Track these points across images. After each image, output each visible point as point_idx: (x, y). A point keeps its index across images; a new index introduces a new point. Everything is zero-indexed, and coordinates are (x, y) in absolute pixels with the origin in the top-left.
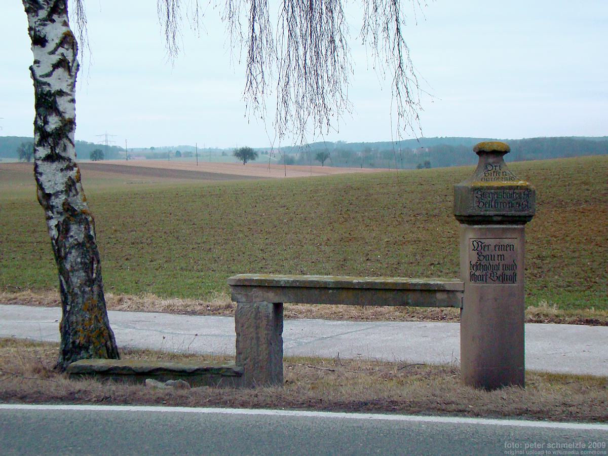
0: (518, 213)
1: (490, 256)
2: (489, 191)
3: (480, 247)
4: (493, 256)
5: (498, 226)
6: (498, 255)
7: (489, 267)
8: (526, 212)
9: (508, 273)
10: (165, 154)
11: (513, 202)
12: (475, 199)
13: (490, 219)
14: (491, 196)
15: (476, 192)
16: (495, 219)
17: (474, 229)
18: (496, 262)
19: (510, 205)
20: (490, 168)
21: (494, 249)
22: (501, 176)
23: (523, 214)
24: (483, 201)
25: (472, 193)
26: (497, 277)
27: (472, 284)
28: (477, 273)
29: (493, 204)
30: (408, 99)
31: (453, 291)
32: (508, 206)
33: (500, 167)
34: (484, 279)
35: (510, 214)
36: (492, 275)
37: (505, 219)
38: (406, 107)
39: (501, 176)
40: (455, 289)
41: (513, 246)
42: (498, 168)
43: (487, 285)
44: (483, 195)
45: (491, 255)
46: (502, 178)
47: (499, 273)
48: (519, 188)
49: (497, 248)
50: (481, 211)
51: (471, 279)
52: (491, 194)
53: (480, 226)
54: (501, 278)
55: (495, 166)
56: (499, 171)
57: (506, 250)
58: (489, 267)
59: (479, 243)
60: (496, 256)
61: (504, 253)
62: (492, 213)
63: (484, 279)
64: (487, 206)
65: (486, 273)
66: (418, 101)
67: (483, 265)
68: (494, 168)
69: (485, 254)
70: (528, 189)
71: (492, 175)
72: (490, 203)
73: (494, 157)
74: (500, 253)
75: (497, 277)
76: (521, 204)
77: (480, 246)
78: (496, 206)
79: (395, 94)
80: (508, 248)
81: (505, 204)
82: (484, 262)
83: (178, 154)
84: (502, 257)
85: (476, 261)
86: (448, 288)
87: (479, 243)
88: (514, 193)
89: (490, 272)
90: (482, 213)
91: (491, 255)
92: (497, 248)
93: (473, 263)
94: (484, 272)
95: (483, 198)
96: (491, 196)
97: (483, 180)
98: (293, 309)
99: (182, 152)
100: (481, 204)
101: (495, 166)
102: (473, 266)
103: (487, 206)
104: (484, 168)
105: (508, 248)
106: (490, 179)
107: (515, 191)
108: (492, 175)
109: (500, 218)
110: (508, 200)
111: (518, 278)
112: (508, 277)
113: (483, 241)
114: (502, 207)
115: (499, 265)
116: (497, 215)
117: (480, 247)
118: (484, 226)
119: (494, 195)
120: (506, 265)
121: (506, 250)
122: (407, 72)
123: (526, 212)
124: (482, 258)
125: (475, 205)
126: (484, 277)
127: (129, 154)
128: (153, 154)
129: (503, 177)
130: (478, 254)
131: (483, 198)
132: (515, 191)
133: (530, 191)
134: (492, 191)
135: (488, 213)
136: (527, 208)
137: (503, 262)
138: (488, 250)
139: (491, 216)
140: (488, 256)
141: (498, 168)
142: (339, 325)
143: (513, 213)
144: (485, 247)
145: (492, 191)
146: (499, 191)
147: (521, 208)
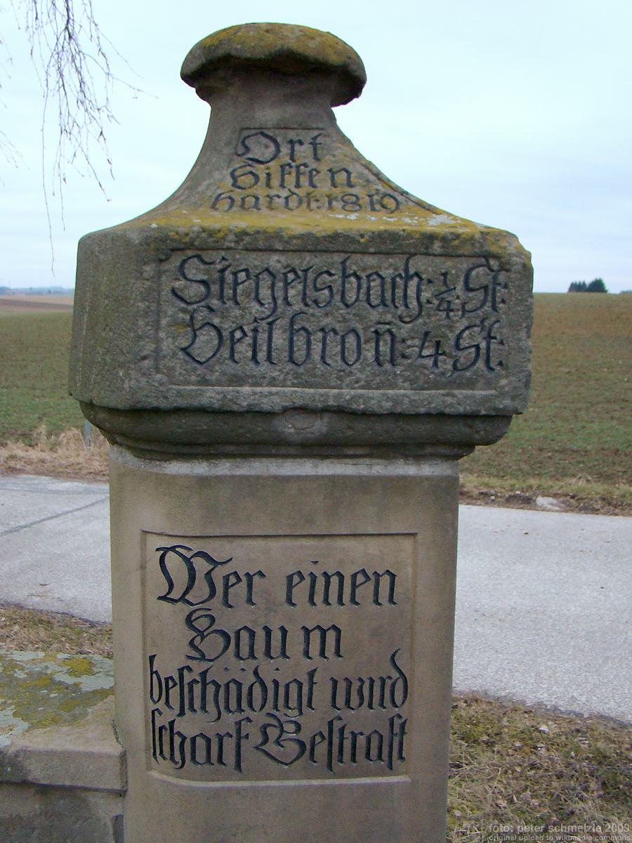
0: (435, 399)
1: (261, 635)
2: (254, 261)
3: (201, 590)
4: (278, 635)
5: (306, 468)
6: (307, 632)
7: (257, 690)
8: (479, 393)
9: (363, 720)
10: (40, 292)
11: (403, 330)
12: (172, 309)
13: (259, 427)
14: (265, 293)
15: (176, 261)
16: (289, 428)
17: (161, 479)
18: (292, 668)
19: (385, 348)
20: (260, 149)
21: (282, 595)
22: (324, 187)
23: (462, 399)
24: (216, 321)
25: (149, 269)
26: (302, 744)
27: (161, 774)
28: (189, 726)
29: (279, 339)
30: (81, 96)
31: (70, 791)
32: (370, 354)
33: (314, 144)
34: (229, 757)
35: (377, 399)
36: (273, 733)
37: (344, 428)
38: (80, 116)
39: (324, 187)
40: (80, 784)
41: (393, 576)
42: (304, 152)
43: (246, 784)
44: (217, 285)
45: (268, 632)
46: (331, 199)
47: (313, 722)
48: (437, 247)
49: (300, 593)
50: (204, 382)
51: (157, 750)
52: (266, 281)
53: (200, 468)
54: (321, 749)
55: (291, 142)
56: (313, 165)
57: (353, 600)
58: (257, 690)
59: (199, 564)
60: (296, 639)
61: (339, 615)
62: (272, 396)
63: (229, 757)
64: (244, 349)
65: (239, 723)
66: (104, 103)
67: (222, 682)
68: (285, 150)
69: (230, 621)
70: (487, 256)
71: (275, 182)
72: (263, 337)
73: (287, 99)
74: (320, 615)
75: (302, 744)
76: (448, 346)
77: (200, 575)
78: (300, 355)
79: (52, 84)
80: (365, 592)
81: (351, 339)
82: (229, 668)
83: (49, 292)
84: (331, 636)
85: (182, 662)
86: (37, 773)
87: (199, 564)
88: (408, 278)
89: (259, 718)
90: (211, 396)
91: (268, 632)
92: (300, 593)
93: (168, 666)
94: (230, 720)
95: (215, 303)
96: (265, 293)
97: (224, 204)
98: (23, 458)
99: (52, 290)
100: (207, 339)
101: (291, 142)
102: (165, 685)
103: (244, 349)
104: (228, 150)
105: (365, 592)
106: (263, 201)
107: (418, 264)
108: (275, 182)
109: (319, 426)
110: (374, 315)
111: (416, 742)
112: (361, 740)
113: (218, 550)
114: (335, 362)
115: (312, 683)
116: (303, 410)
117: (201, 590)
118: (224, 468)
119: (287, 284)
120: (349, 682)
121: (353, 600)
122: (82, 37)
123: (479, 393)
124: (212, 645)
125: (167, 345)
126: (229, 744)
127: (14, 292)
128: (31, 292)
129: (337, 192)
130: (189, 621)
131: (215, 303)
132: (418, 264)
133: (505, 267)
134: (275, 261)
135: (246, 394)
136: (480, 364)
137: (329, 668)
138: (250, 601)
139: (270, 414)
140: (252, 634)
141: (304, 152)
142: (67, 492)
143: (403, 395)
144: (221, 589)
145: (275, 261)
146: (318, 261)
147: (446, 364)
